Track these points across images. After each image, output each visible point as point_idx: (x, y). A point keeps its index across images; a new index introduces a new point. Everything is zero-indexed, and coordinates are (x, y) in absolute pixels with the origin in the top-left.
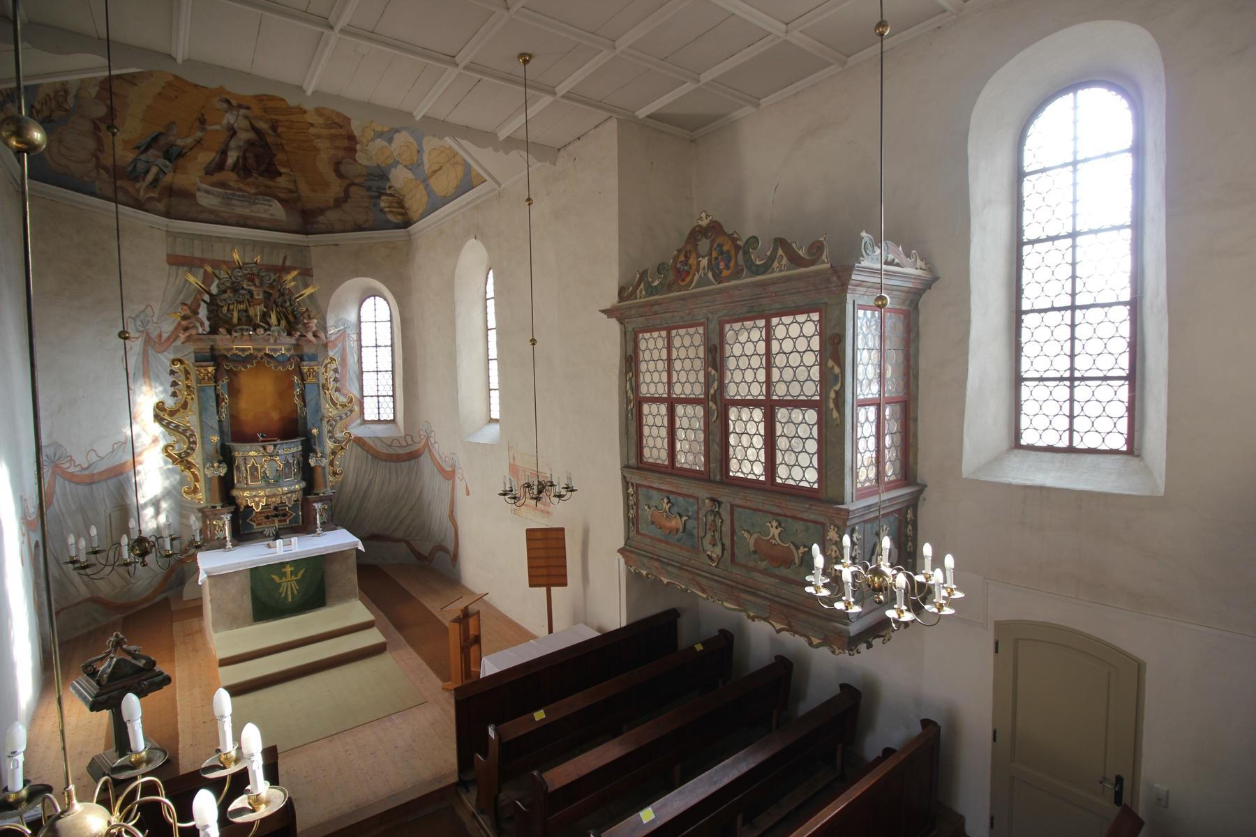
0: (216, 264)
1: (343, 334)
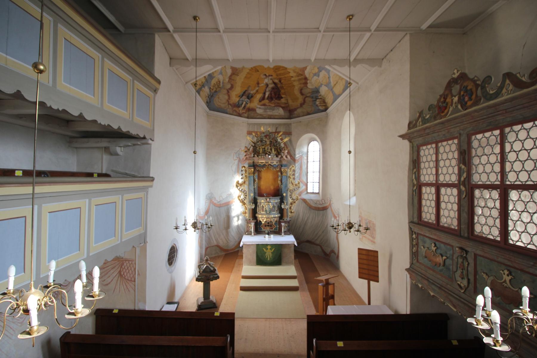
0: (256, 133)
1: (301, 157)
